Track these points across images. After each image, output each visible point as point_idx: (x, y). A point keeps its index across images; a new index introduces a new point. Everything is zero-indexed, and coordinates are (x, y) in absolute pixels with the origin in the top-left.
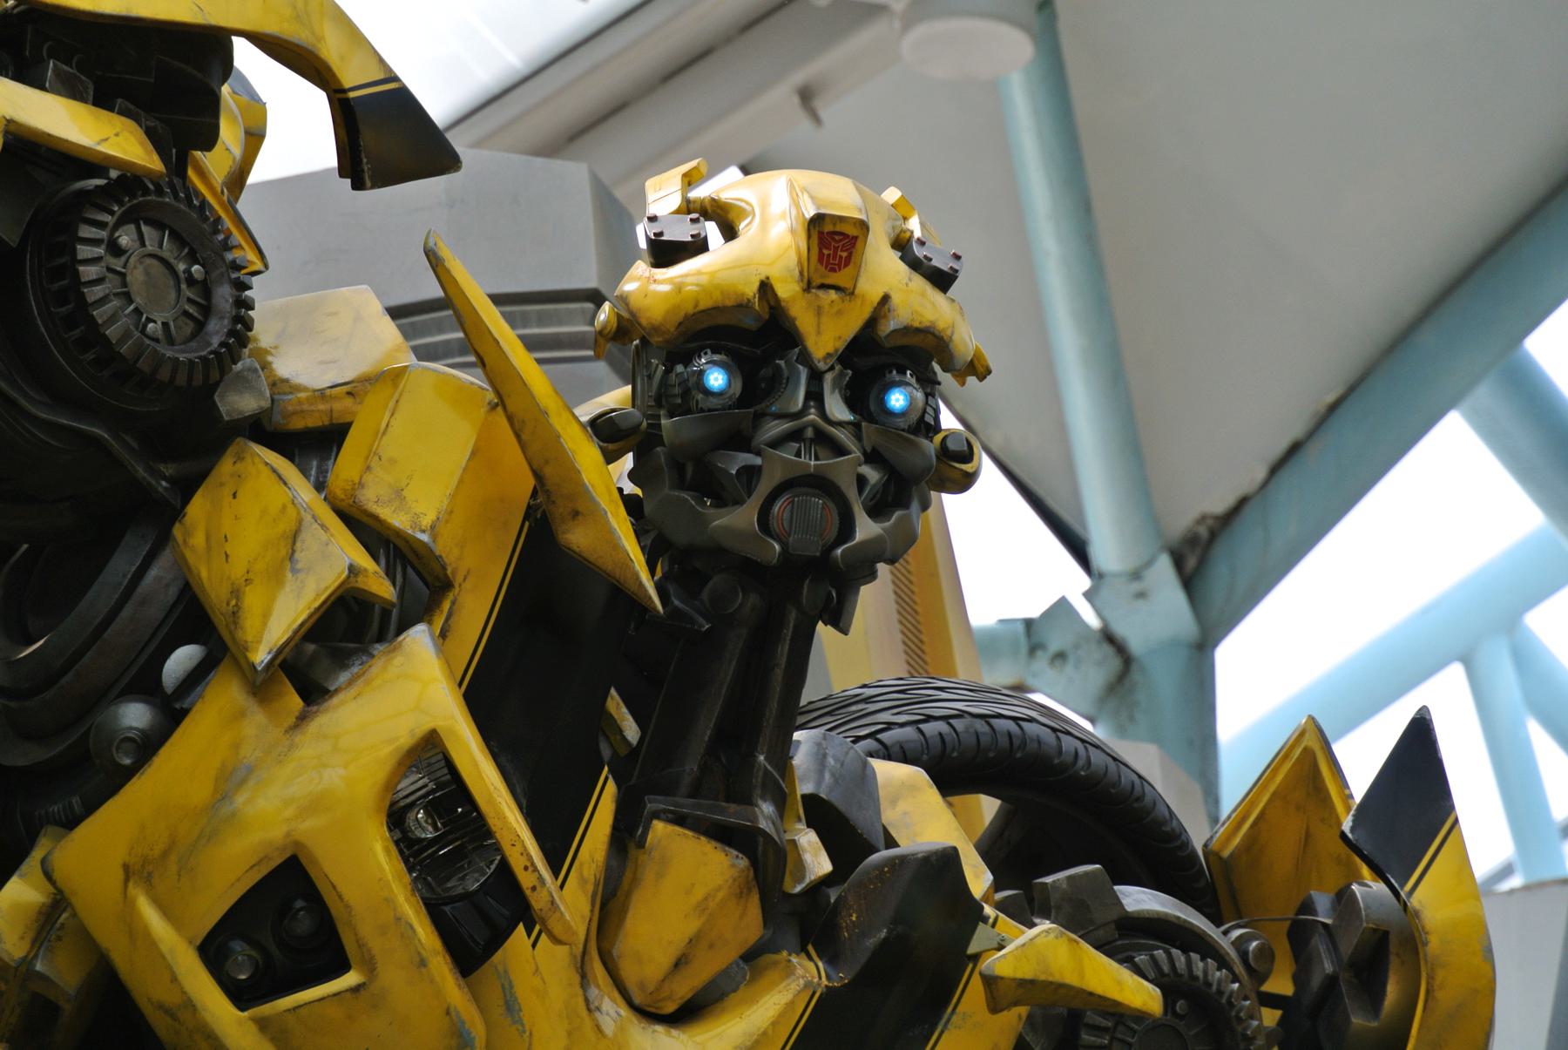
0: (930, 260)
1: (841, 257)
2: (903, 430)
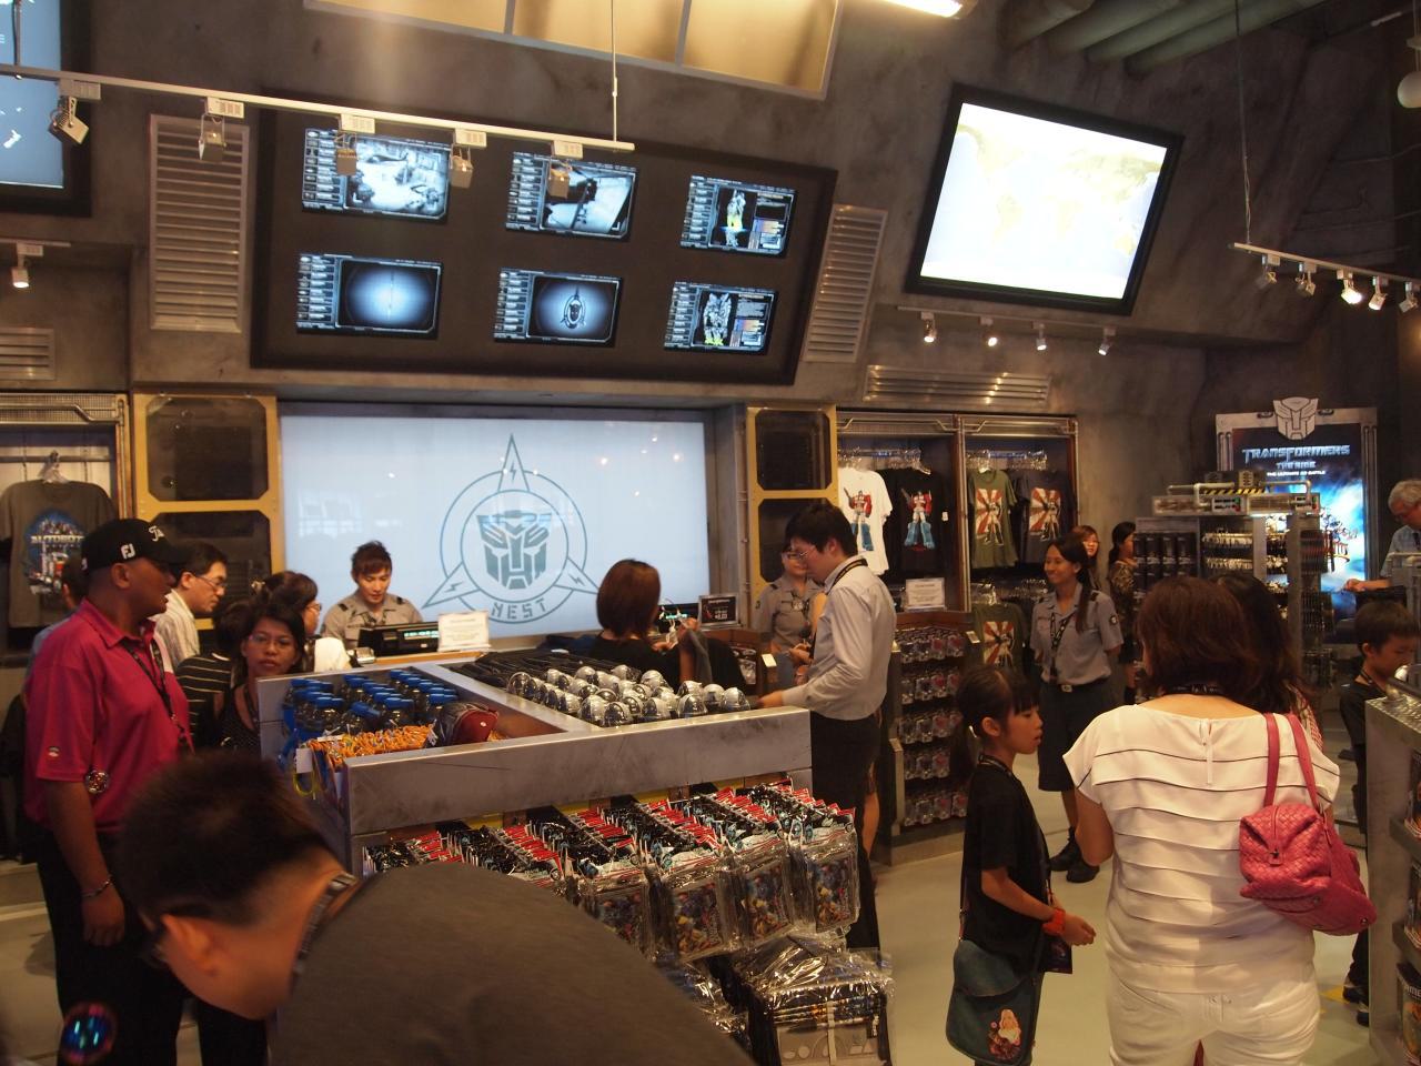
0: (1259, 416)
1: (527, 557)
2: (859, 823)
